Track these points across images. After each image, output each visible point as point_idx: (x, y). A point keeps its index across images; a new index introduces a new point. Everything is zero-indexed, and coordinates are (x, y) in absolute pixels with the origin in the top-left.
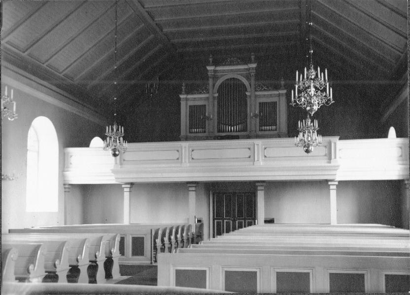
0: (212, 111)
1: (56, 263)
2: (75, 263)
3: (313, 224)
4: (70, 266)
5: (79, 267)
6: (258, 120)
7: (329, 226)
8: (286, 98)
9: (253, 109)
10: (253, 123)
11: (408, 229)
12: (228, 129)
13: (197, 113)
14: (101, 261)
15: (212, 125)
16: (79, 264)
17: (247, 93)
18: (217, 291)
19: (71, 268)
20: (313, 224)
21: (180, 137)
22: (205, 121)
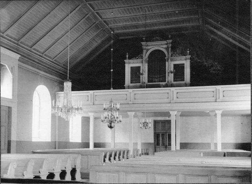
0: (144, 68)
1: (24, 173)
2: (64, 169)
3: (38, 51)
4: (34, 176)
5: (54, 173)
6: (173, 74)
7: (21, 66)
8: (190, 61)
9: (170, 66)
10: (170, 78)
11: (250, 150)
12: (153, 80)
13: (136, 72)
14: (45, 175)
15: (145, 78)
16: (76, 167)
17: (166, 58)
18: (250, 88)
19: (49, 173)
20: (38, 51)
21: (125, 86)
22: (140, 76)
